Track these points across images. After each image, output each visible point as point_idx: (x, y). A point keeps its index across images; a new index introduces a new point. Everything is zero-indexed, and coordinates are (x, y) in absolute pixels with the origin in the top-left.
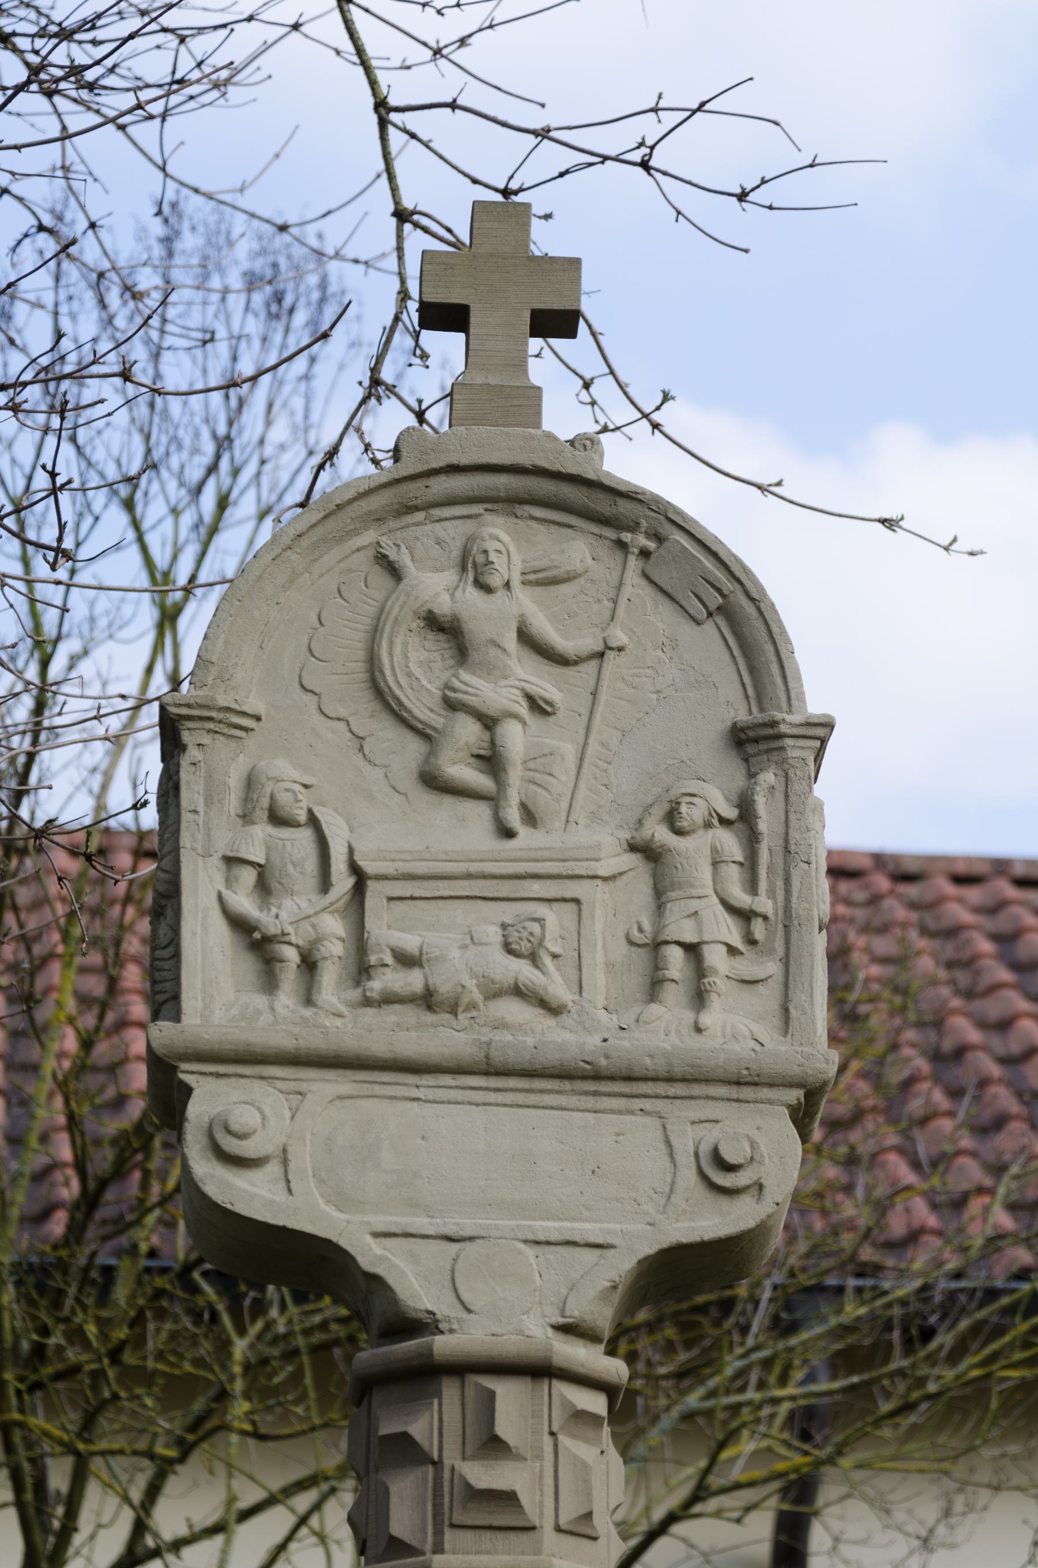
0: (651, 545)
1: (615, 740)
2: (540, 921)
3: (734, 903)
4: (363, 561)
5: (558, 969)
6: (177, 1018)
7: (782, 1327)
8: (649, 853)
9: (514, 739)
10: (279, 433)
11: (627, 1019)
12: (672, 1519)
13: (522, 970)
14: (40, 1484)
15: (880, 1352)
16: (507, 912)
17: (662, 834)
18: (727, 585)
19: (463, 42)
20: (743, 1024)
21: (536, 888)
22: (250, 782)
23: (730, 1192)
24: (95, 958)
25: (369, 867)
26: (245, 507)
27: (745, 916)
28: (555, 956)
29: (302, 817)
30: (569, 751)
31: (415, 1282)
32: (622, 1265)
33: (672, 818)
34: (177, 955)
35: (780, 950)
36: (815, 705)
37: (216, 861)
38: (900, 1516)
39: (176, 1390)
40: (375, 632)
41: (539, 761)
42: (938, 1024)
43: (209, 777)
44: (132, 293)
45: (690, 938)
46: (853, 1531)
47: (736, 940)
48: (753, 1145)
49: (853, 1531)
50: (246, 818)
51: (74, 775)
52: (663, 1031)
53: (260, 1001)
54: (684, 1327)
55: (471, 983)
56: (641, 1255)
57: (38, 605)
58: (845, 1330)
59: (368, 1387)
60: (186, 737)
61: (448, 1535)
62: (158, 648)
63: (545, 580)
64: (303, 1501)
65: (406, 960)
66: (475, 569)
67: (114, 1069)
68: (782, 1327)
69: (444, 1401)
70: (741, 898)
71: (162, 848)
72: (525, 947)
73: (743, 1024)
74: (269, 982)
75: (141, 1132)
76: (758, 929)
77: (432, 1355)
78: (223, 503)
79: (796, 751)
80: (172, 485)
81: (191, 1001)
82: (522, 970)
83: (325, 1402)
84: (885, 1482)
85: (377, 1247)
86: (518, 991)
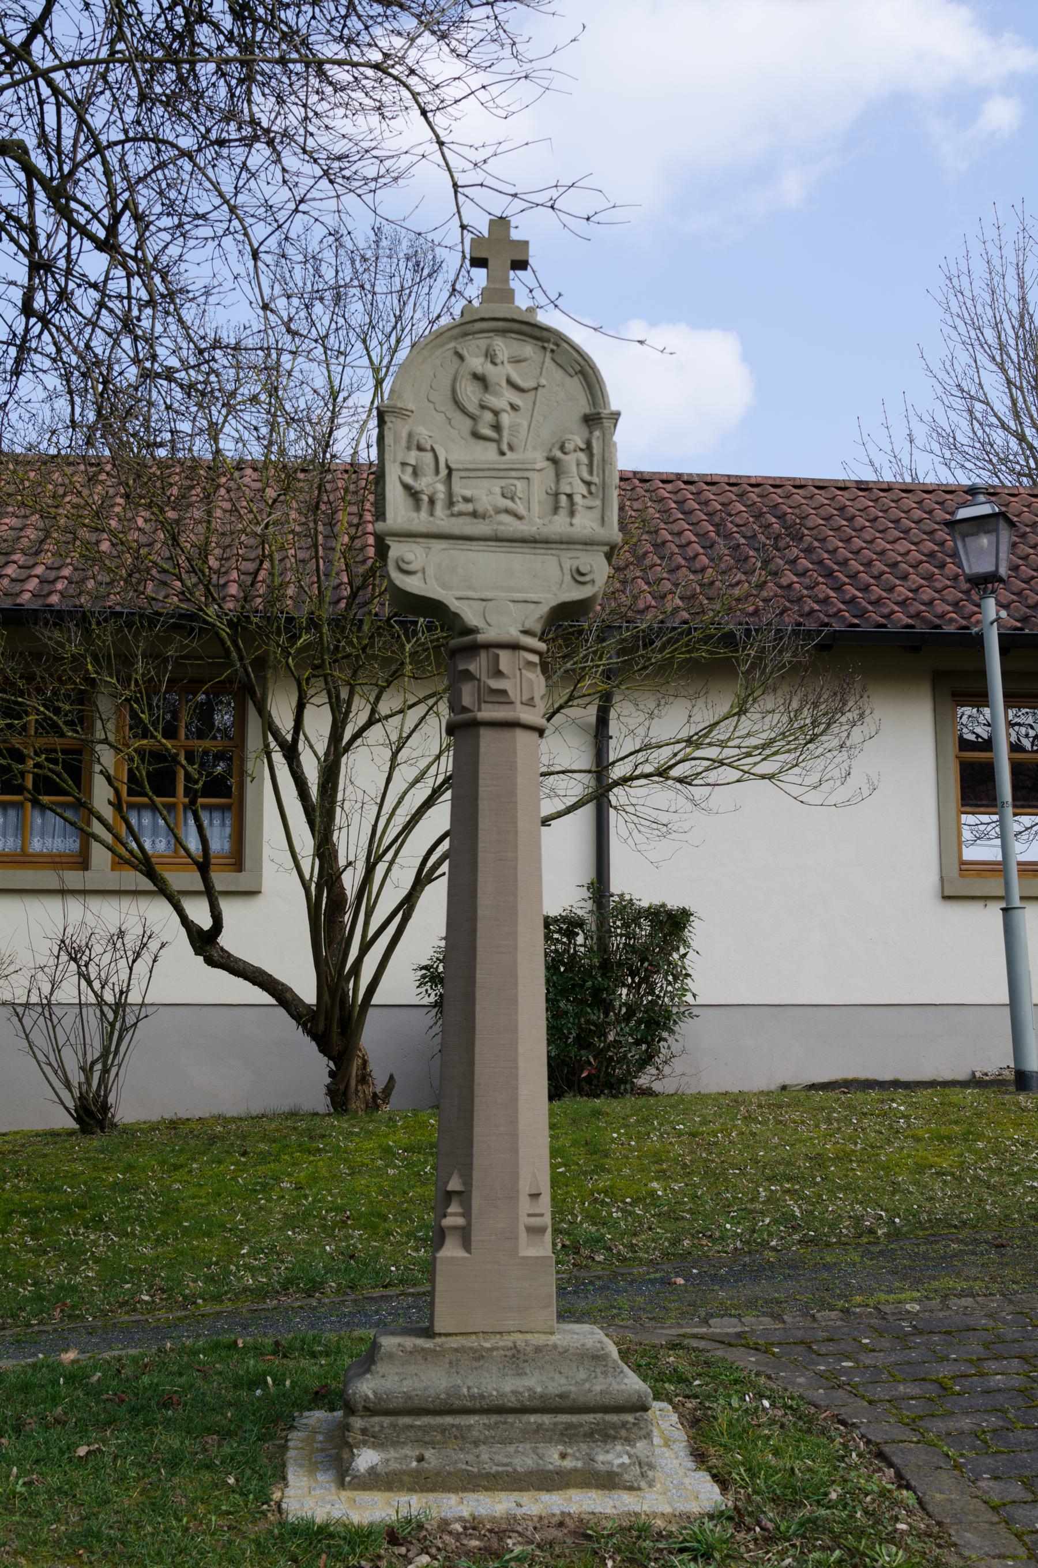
1: (539, 421)
4: (450, 353)
6: (384, 520)
7: (600, 640)
8: (554, 461)
9: (506, 419)
10: (418, 315)
11: (546, 521)
12: (561, 707)
13: (509, 504)
14: (338, 696)
15: (635, 648)
16: (503, 483)
17: (558, 454)
18: (583, 363)
19: (485, 161)
20: (588, 523)
21: (513, 474)
22: (410, 435)
23: (583, 583)
24: (354, 509)
25: (453, 466)
26: (407, 343)
27: (588, 484)
30: (525, 424)
31: (471, 616)
32: (544, 609)
33: (562, 448)
34: (384, 499)
36: (614, 407)
37: (398, 464)
38: (642, 707)
39: (386, 662)
40: (454, 380)
41: (514, 427)
42: (656, 532)
43: (395, 434)
44: (364, 259)
45: (569, 492)
46: (625, 712)
47: (585, 493)
49: (625, 712)
50: (409, 448)
51: (346, 441)
52: (559, 526)
53: (414, 515)
54: (565, 640)
55: (490, 508)
57: (327, 66)
58: (624, 640)
59: (454, 653)
60: (387, 419)
61: (483, 705)
62: (375, 395)
63: (516, 361)
64: (431, 702)
65: (467, 500)
66: (490, 356)
67: (362, 549)
68: (600, 640)
70: (587, 477)
71: (379, 476)
73: (588, 523)
74: (418, 507)
75: (372, 570)
76: (593, 489)
78: (398, 341)
79: (607, 423)
80: (380, 334)
81: (389, 515)
82: (509, 504)
83: (438, 665)
84: (636, 694)
85: (457, 603)
86: (507, 511)
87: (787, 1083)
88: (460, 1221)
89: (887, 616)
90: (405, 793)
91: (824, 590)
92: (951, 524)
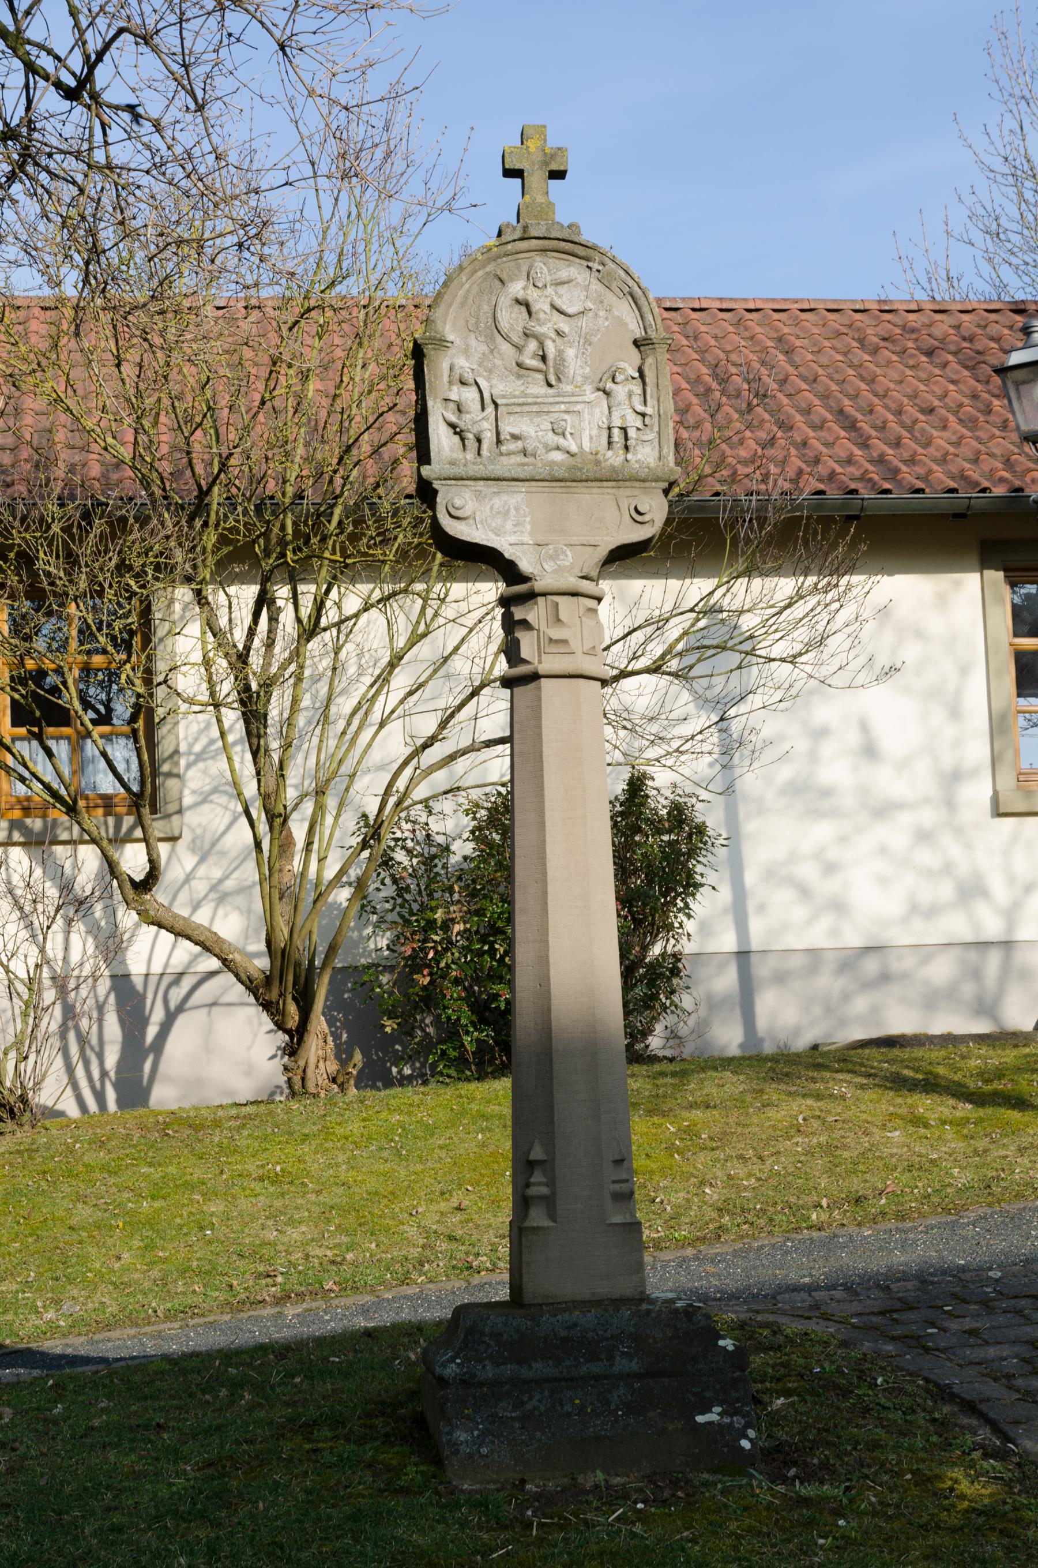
13: (561, 441)
17: (609, 385)
18: (631, 283)
29: (472, 381)
35: (656, 429)
47: (641, 426)
61: (544, 656)
65: (515, 437)
70: (640, 408)
87: (819, 1042)
88: (544, 1190)
89: (925, 478)
90: (464, 752)
91: (846, 446)
92: (1002, 371)
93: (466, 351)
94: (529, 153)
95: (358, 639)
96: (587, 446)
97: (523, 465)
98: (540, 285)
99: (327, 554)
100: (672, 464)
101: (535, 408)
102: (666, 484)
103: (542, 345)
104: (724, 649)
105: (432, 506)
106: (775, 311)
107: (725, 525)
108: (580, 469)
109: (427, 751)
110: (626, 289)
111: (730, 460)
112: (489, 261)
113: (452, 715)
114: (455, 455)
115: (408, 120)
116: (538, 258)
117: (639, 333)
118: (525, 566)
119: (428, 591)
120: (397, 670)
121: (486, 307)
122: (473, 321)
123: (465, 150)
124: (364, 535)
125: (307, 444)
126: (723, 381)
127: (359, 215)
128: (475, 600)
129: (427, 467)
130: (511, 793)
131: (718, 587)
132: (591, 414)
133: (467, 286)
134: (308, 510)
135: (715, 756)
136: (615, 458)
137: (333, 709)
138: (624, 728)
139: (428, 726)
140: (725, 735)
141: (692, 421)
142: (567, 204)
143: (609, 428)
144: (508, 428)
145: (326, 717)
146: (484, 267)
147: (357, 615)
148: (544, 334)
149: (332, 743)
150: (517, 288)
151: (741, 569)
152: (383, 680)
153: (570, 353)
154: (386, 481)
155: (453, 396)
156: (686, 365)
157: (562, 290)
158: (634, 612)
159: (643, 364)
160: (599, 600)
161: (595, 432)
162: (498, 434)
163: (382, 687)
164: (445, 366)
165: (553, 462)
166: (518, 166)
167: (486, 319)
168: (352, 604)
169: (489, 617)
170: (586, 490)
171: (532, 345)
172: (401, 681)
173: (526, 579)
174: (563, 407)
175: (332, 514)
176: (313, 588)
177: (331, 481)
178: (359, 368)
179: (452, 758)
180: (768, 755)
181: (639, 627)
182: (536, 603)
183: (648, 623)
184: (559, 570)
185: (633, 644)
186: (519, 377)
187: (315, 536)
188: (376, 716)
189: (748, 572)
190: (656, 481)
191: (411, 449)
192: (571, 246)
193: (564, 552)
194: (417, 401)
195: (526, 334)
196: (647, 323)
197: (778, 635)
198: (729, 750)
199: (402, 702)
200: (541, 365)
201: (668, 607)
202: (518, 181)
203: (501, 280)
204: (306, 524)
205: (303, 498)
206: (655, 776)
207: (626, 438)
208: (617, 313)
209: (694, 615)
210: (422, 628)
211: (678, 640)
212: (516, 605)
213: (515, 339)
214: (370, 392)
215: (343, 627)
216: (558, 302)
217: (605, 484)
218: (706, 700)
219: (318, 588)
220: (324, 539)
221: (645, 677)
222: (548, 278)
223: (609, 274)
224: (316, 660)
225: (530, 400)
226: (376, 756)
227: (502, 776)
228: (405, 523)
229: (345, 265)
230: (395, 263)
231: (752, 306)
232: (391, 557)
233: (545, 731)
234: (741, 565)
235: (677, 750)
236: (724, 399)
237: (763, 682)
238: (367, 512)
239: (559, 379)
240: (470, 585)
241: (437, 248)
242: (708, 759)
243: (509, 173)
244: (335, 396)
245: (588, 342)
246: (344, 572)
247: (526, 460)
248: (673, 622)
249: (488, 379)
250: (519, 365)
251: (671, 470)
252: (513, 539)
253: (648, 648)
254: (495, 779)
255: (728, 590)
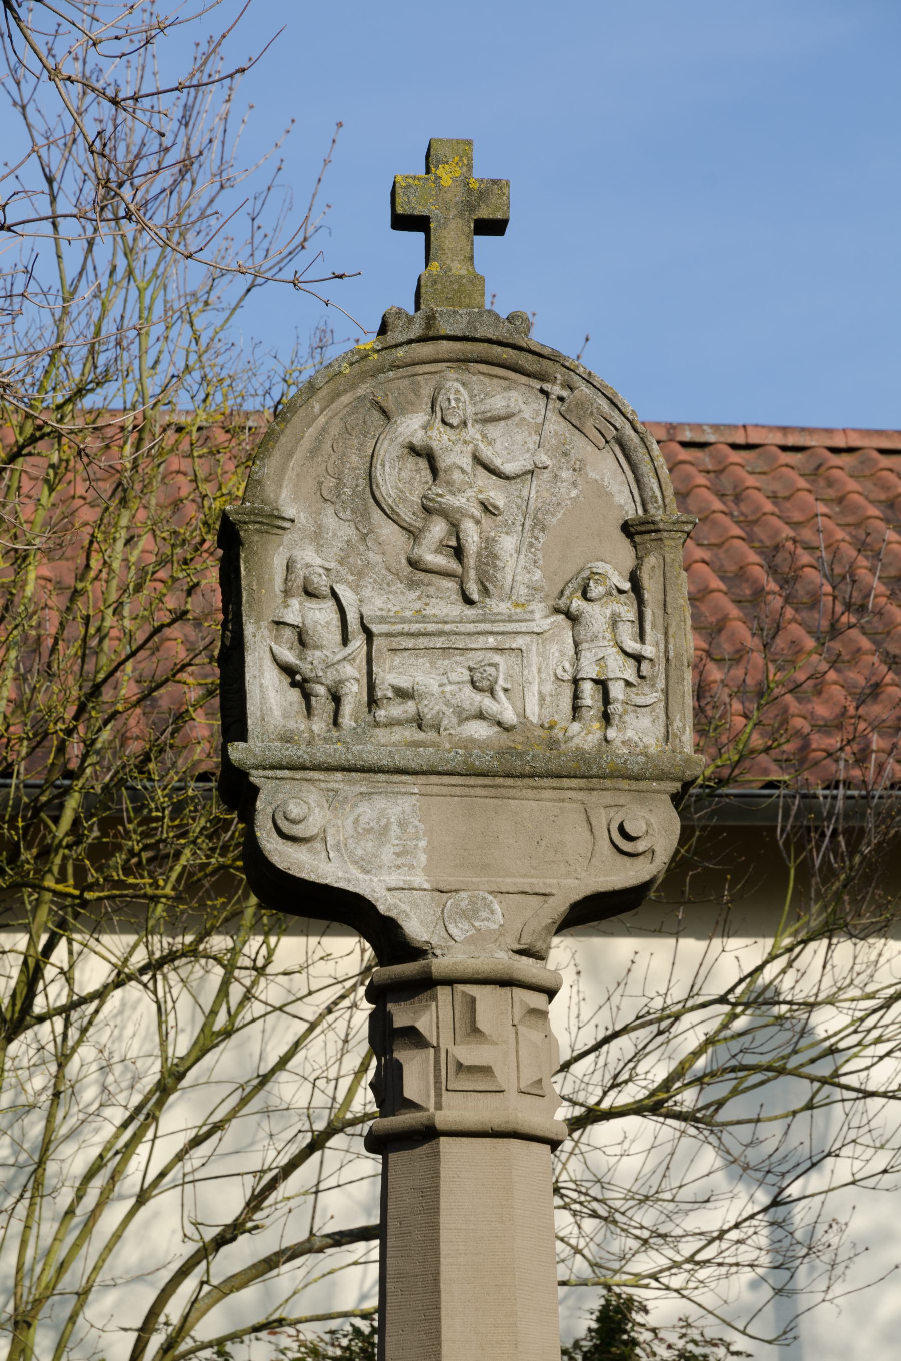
0: (565, 393)
2: (495, 666)
3: (629, 650)
5: (508, 699)
13: (487, 702)
17: (577, 604)
18: (619, 421)
28: (506, 690)
29: (326, 591)
35: (661, 684)
47: (633, 679)
48: (648, 824)
56: (572, 901)
61: (446, 1096)
65: (403, 694)
69: (440, 1004)
70: (632, 646)
72: (485, 684)
77: (431, 973)
93: (318, 537)
94: (440, 188)
95: (104, 1038)
96: (533, 712)
97: (416, 744)
98: (455, 421)
99: (49, 882)
100: (689, 749)
101: (440, 642)
102: (678, 785)
103: (455, 528)
104: (782, 1071)
105: (248, 815)
106: (883, 451)
107: (787, 843)
108: (520, 755)
109: (225, 1250)
110: (611, 433)
111: (798, 722)
112: (363, 376)
113: (272, 1185)
114: (292, 724)
115: (226, 106)
116: (452, 374)
117: (631, 511)
118: (416, 928)
119: (235, 952)
120: (172, 1098)
121: (355, 459)
122: (331, 482)
123: (326, 162)
124: (118, 848)
125: (20, 679)
126: (788, 580)
127: (130, 273)
128: (322, 972)
129: (241, 744)
130: (380, 1331)
131: (772, 958)
132: (543, 655)
133: (322, 419)
134: (18, 799)
135: (760, 1271)
136: (584, 735)
137: (51, 1167)
138: (594, 1215)
139: (226, 1202)
140: (780, 1233)
141: (727, 649)
142: (507, 279)
143: (576, 681)
144: (389, 676)
145: (38, 1184)
146: (354, 386)
147: (101, 995)
148: (459, 510)
149: (48, 1229)
150: (412, 426)
151: (814, 924)
152: (146, 1115)
153: (507, 544)
154: (161, 751)
155: (292, 617)
156: (719, 546)
157: (495, 431)
158: (615, 999)
159: (638, 567)
160: (551, 993)
161: (548, 687)
162: (372, 687)
163: (143, 1128)
164: (278, 563)
165: (471, 740)
166: (420, 210)
167: (354, 480)
168: (93, 974)
169: (346, 1003)
170: (529, 793)
171: (438, 529)
172: (179, 1118)
173: (416, 953)
174: (491, 641)
175: (61, 806)
176: (21, 941)
177: (61, 749)
178: (120, 544)
179: (271, 1263)
180: (864, 1269)
181: (625, 1030)
182: (435, 998)
183: (641, 1021)
184: (478, 938)
185: (612, 1059)
186: (412, 584)
187: (28, 847)
188: (131, 1182)
189: (829, 930)
190: (659, 779)
191: (210, 693)
192: (512, 354)
193: (488, 906)
194: (224, 625)
195: (427, 510)
196: (648, 494)
197: (883, 1048)
198: (788, 1258)
199: (180, 1157)
200: (453, 565)
201: (678, 993)
202: (421, 236)
203: (384, 412)
204: (12, 825)
205: (10, 776)
206: (650, 1305)
207: (606, 699)
208: (592, 475)
209: (727, 1008)
210: (221, 1020)
211: (696, 1054)
212: (397, 1001)
213: (407, 517)
214: (138, 588)
215: (74, 1015)
216: (486, 453)
217: (566, 782)
218: (746, 1168)
219: (32, 942)
220: (45, 854)
221: (633, 1120)
222: (470, 410)
223: (580, 404)
224: (23, 1074)
225: (431, 628)
226: (128, 1256)
227: (364, 1298)
228: (196, 828)
229: (101, 360)
230: (193, 357)
231: (840, 442)
232: (168, 891)
233: (444, 1235)
234: (815, 918)
235: (691, 1260)
236: (789, 612)
237: (852, 1134)
238: (127, 804)
239: (485, 591)
240: (313, 940)
241: (270, 342)
242: (747, 1275)
243: (402, 222)
244: (76, 594)
245: (540, 525)
246: (80, 914)
247: (421, 736)
248: (688, 1020)
249: (356, 588)
250: (413, 563)
251: (688, 760)
252: (394, 879)
253: (641, 1069)
254: (348, 1303)
255: (790, 965)
